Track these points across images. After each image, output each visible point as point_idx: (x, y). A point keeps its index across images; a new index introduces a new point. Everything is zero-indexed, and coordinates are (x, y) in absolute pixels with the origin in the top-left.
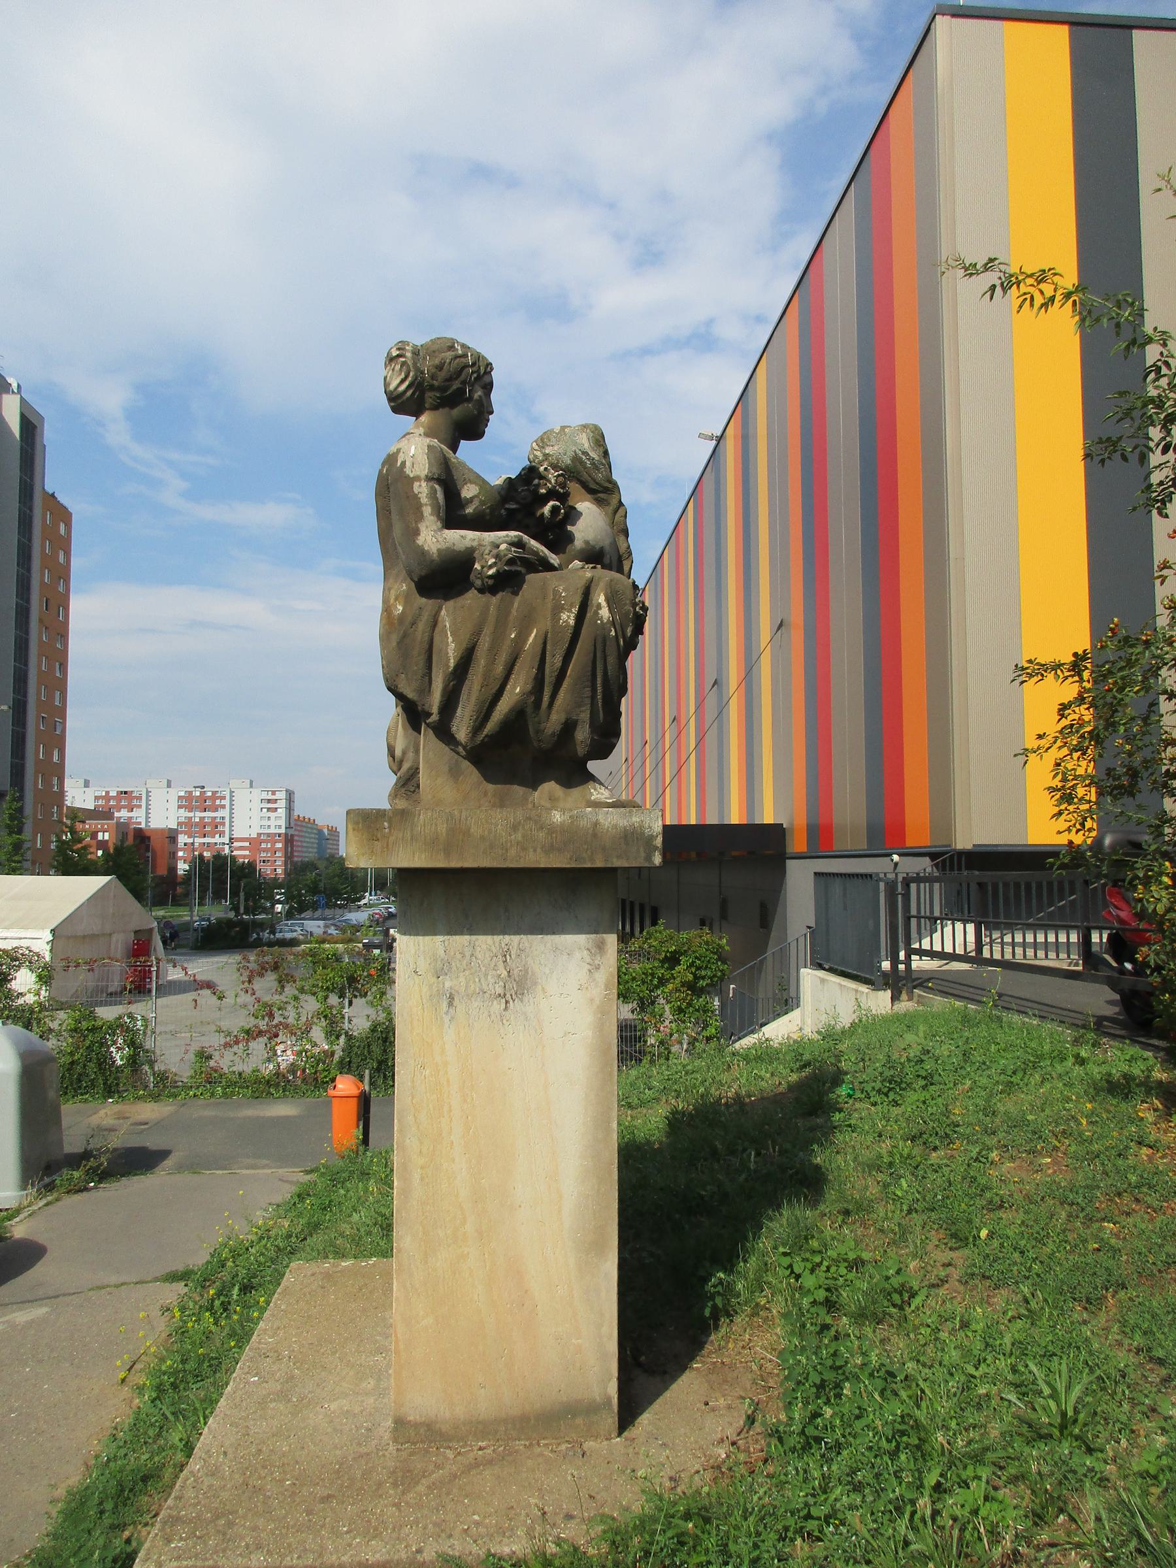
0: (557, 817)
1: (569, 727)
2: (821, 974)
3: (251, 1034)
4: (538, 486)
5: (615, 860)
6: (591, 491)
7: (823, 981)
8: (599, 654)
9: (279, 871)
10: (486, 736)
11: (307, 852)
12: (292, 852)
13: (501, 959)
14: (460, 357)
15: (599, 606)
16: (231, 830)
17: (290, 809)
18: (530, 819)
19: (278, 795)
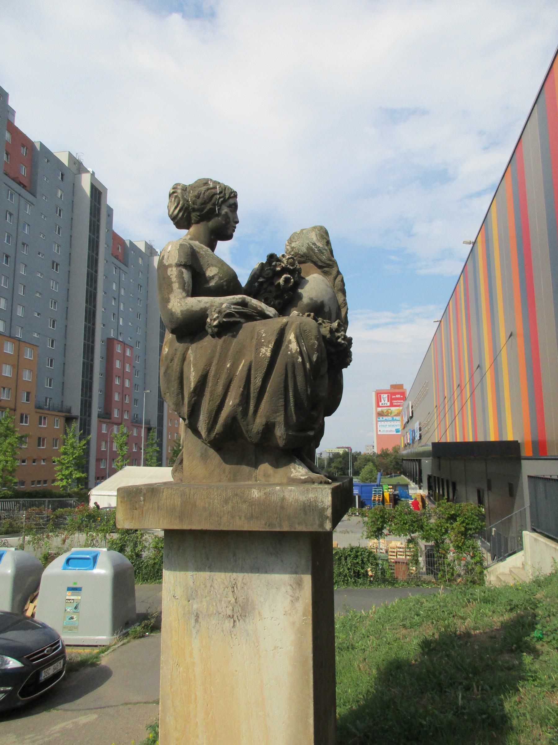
0: (256, 494)
1: (269, 428)
2: (535, 535)
4: (276, 266)
5: (297, 526)
6: (320, 267)
7: (536, 540)
8: (290, 375)
10: (217, 434)
13: (230, 589)
14: (212, 189)
15: (290, 342)
18: (237, 495)
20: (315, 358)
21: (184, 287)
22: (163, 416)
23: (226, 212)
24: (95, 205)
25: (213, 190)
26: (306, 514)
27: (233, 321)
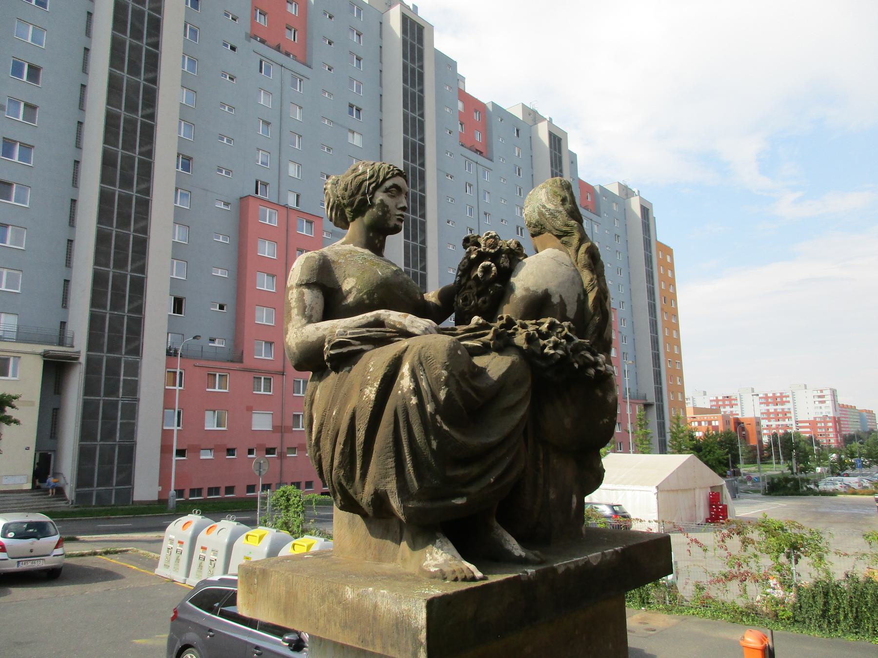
3: (729, 577)
6: (559, 237)
9: (832, 441)
11: (852, 428)
12: (840, 427)
16: (795, 416)
19: (825, 393)
20: (442, 395)
21: (305, 311)
22: (661, 388)
23: (382, 201)
24: (555, 154)
25: (361, 177)
26: (398, 634)
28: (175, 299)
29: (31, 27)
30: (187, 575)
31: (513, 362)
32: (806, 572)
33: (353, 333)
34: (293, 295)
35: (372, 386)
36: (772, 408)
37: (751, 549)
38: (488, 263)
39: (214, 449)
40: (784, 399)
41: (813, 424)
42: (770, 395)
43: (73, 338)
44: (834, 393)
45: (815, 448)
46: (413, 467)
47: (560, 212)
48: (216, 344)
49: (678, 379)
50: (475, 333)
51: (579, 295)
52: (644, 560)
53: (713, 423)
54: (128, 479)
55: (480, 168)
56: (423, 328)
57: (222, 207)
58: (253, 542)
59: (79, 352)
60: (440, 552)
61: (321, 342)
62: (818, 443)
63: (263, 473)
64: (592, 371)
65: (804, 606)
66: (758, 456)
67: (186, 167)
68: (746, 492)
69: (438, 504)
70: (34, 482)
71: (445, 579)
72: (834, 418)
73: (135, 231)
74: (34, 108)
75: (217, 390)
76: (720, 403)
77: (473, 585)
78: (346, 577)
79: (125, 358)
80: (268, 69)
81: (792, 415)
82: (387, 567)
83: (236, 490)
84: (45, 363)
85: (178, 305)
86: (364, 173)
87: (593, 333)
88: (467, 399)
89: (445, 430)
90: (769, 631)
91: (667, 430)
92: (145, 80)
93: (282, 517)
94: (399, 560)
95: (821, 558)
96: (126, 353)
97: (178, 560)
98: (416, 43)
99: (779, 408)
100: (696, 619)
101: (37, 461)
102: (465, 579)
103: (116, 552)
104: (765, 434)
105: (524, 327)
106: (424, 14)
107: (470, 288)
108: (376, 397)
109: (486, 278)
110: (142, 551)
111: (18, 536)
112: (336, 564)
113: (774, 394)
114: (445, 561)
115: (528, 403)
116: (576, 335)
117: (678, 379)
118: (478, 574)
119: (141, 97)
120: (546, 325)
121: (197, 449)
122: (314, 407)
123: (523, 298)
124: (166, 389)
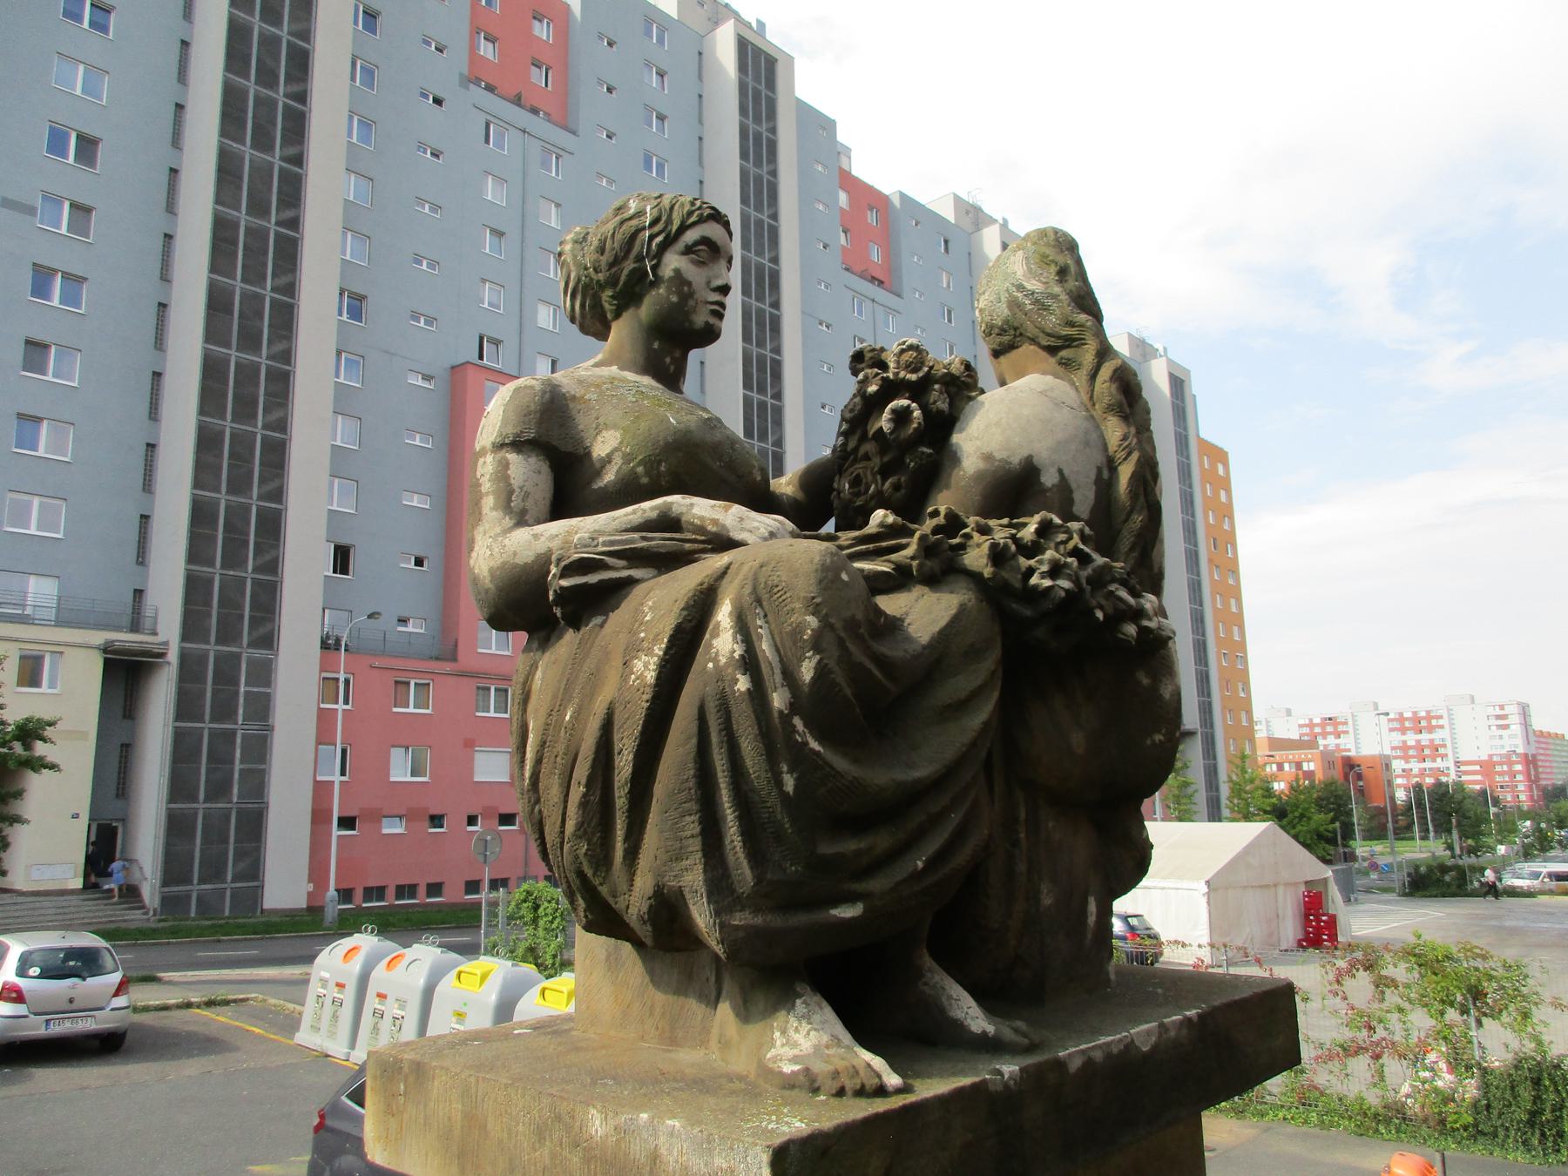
3: (1350, 1050)
6: (1052, 350)
9: (1523, 797)
12: (1537, 773)
16: (1455, 753)
17: (1526, 724)
20: (807, 671)
21: (509, 500)
22: (1210, 704)
23: (677, 272)
25: (634, 222)
27: (601, 581)
28: (337, 548)
29: (81, 68)
30: (353, 1045)
31: (962, 610)
32: (1498, 1043)
33: (612, 543)
34: (486, 467)
35: (649, 652)
36: (1411, 738)
37: (1392, 998)
38: (904, 402)
39: (408, 816)
40: (1434, 722)
41: (1487, 767)
42: (1408, 714)
43: (155, 618)
44: (1524, 711)
45: (1493, 810)
46: (742, 834)
47: (1055, 297)
48: (410, 628)
49: (1240, 686)
50: (877, 546)
51: (1099, 470)
52: (1243, 1037)
53: (1305, 767)
54: (253, 870)
55: (879, 309)
56: (764, 532)
57: (420, 383)
58: (470, 985)
59: (166, 643)
60: (805, 1027)
61: (543, 562)
62: (1496, 802)
63: (491, 858)
64: (1131, 630)
65: (1495, 1104)
66: (1390, 825)
67: (356, 313)
68: (1368, 891)
69: (801, 919)
70: (86, 876)
71: (816, 1091)
72: (1526, 755)
73: (265, 427)
74: (87, 210)
75: (411, 710)
76: (1317, 730)
77: (880, 1106)
78: (594, 1083)
79: (247, 654)
80: (500, 136)
81: (1449, 750)
82: (688, 1057)
83: (446, 889)
84: (107, 662)
85: (342, 559)
86: (640, 214)
87: (1132, 549)
88: (865, 688)
89: (812, 750)
90: (1438, 1156)
91: (1222, 777)
92: (282, 159)
93: (526, 936)
94: (714, 1044)
95: (1526, 1015)
96: (249, 646)
97: (335, 1017)
98: (762, 87)
99: (1425, 738)
100: (1290, 1128)
101: (93, 838)
102: (861, 1092)
103: (226, 1003)
104: (1399, 786)
105: (984, 530)
106: (777, 38)
107: (867, 457)
108: (658, 678)
109: (903, 427)
110: (273, 1001)
111: (46, 974)
112: (577, 1049)
113: (1415, 713)
114: (817, 1048)
115: (996, 695)
116: (1097, 550)
117: (1240, 686)
118: (893, 1080)
119: (275, 189)
120: (1032, 528)
121: (376, 816)
122: (531, 707)
123: (979, 476)
124: (320, 710)
